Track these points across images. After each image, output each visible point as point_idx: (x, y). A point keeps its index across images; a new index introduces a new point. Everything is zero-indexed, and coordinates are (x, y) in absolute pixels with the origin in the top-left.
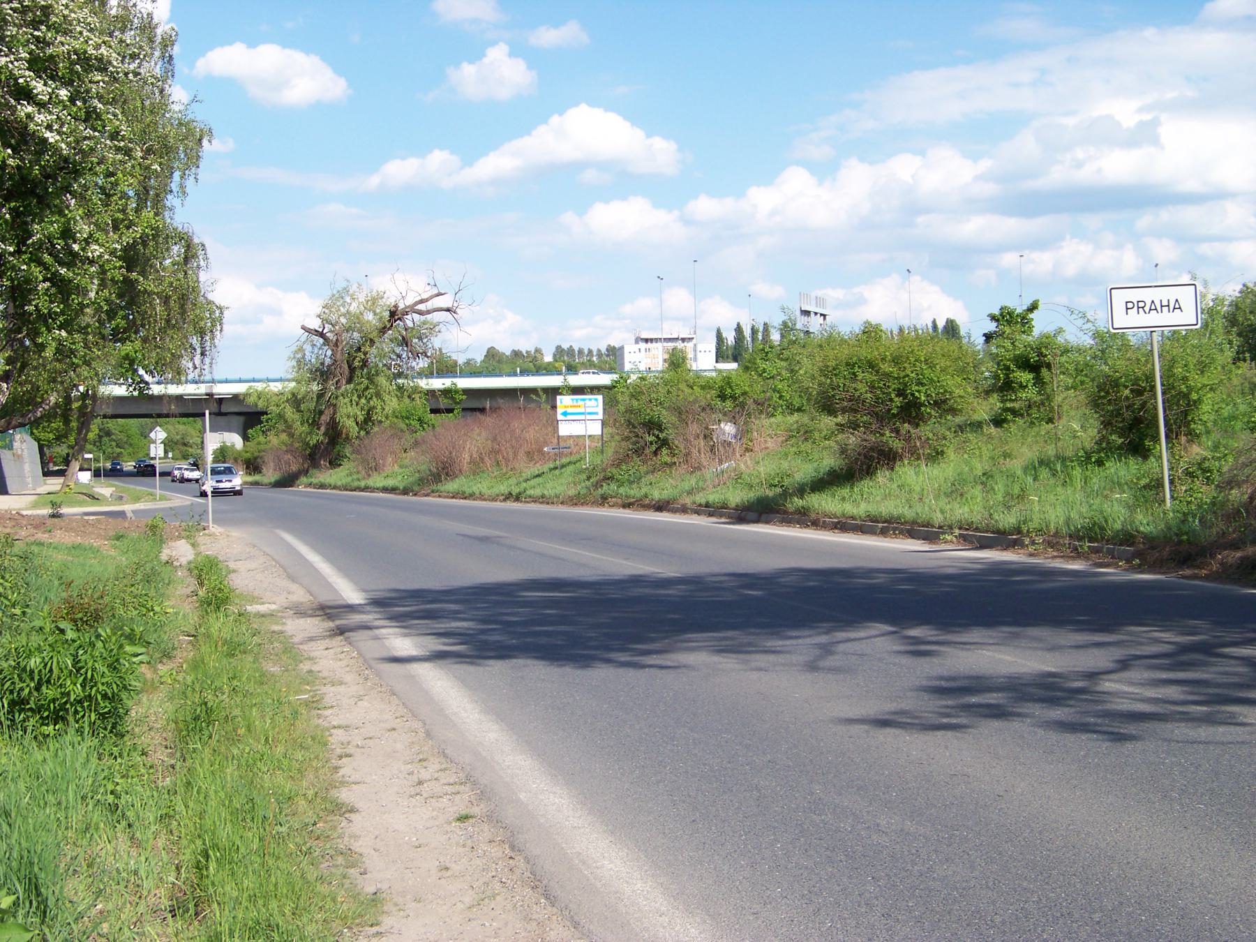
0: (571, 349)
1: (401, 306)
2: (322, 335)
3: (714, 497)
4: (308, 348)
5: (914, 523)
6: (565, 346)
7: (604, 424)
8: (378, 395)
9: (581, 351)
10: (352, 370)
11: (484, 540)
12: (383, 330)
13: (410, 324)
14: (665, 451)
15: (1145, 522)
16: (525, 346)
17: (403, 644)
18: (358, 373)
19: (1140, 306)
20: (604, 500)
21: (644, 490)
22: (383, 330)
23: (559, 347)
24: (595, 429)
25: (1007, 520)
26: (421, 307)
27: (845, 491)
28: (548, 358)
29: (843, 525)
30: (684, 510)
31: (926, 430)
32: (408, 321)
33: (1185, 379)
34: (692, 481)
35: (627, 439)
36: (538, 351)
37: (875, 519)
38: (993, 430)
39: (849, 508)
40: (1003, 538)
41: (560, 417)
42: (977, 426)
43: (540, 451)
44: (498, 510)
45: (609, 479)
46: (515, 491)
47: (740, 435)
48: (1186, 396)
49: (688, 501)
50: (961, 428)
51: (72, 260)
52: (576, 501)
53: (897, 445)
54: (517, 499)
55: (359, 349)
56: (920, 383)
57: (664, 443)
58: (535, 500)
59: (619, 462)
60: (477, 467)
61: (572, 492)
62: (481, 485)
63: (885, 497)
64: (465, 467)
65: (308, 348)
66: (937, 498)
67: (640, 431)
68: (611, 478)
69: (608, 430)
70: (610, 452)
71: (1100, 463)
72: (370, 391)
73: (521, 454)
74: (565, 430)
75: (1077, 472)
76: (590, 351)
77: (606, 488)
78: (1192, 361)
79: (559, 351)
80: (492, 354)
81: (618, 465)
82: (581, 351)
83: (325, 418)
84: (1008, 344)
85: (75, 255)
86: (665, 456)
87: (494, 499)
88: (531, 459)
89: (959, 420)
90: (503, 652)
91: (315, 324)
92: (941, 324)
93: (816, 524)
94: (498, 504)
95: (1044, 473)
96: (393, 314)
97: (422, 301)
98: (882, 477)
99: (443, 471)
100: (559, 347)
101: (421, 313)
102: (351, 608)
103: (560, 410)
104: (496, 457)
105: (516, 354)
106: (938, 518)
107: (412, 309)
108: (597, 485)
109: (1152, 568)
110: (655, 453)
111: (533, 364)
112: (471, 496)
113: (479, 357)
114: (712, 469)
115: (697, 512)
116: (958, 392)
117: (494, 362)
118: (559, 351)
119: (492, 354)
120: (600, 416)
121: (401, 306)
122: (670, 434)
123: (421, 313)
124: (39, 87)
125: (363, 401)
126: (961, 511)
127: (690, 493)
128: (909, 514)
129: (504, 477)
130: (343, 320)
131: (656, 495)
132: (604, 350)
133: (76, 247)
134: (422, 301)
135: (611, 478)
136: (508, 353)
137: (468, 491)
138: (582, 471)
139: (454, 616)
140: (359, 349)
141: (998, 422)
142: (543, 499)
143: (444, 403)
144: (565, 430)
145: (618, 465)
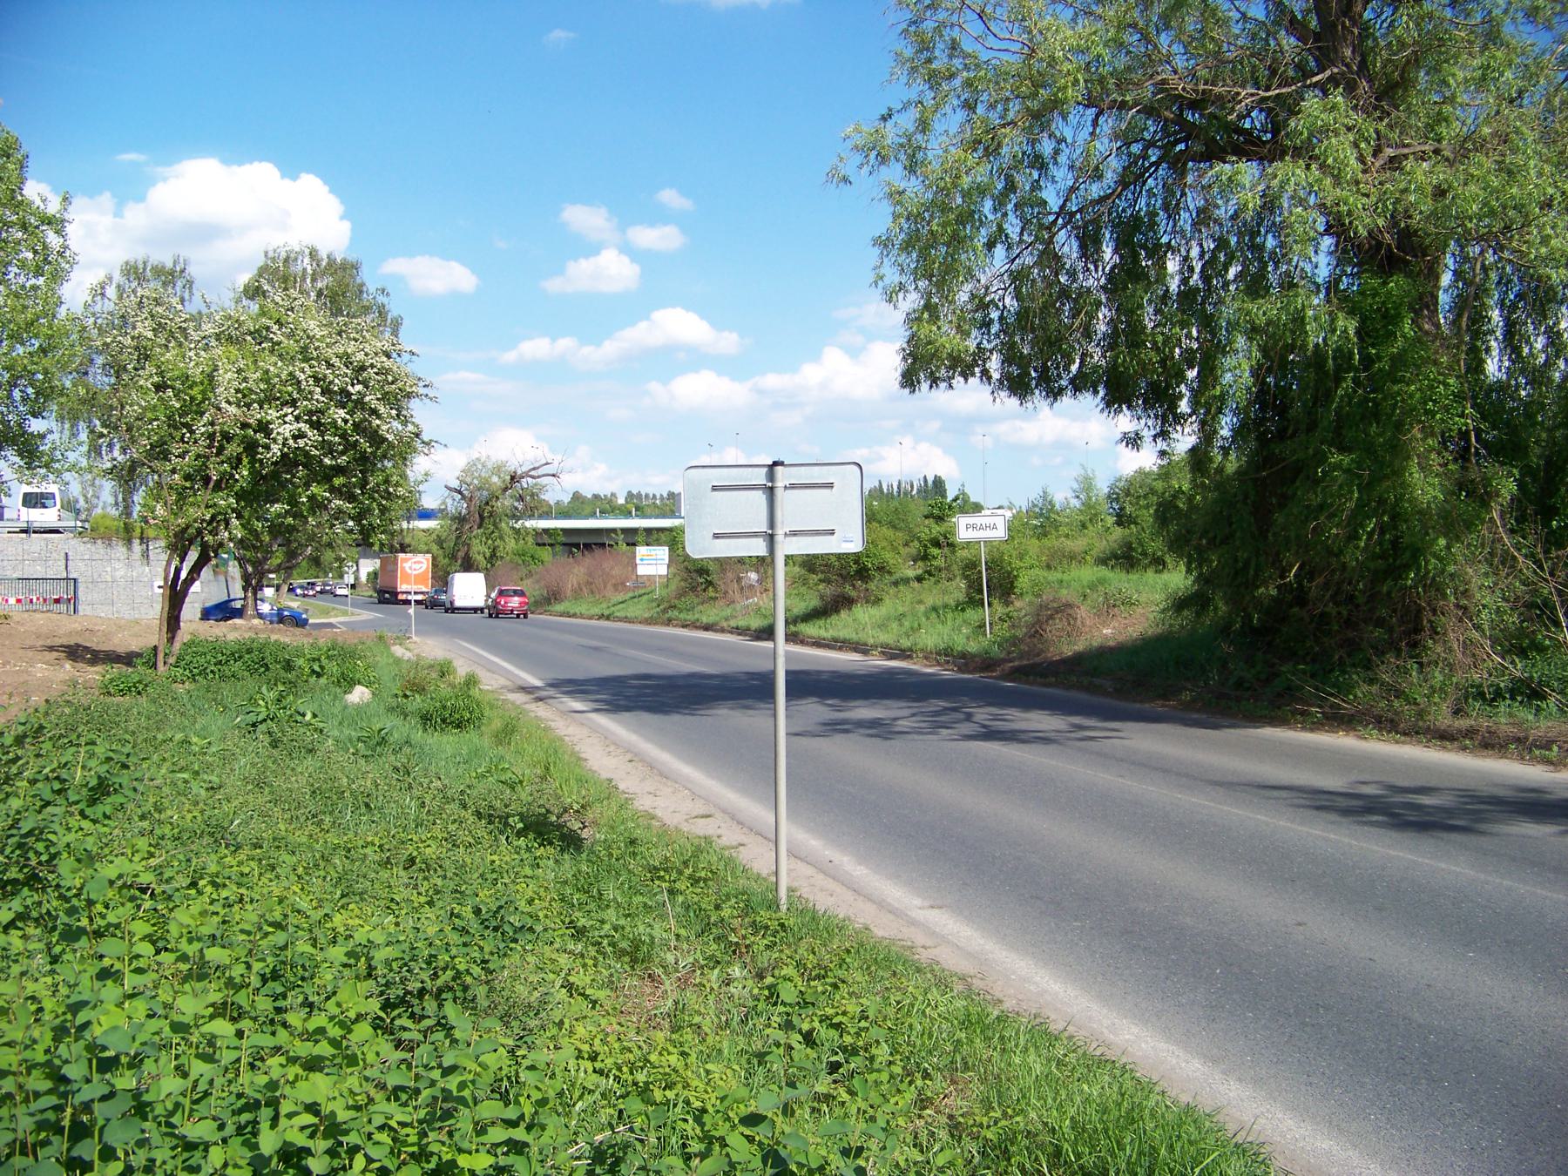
0: (639, 494)
1: (519, 472)
2: (460, 492)
3: (742, 623)
4: (449, 502)
5: (858, 643)
6: (635, 492)
7: (669, 566)
8: (501, 538)
9: (647, 496)
10: (482, 518)
11: (596, 649)
12: (506, 489)
13: (525, 486)
14: (711, 589)
15: (973, 647)
16: (604, 490)
17: (578, 706)
18: (487, 521)
19: (974, 527)
20: (669, 622)
21: (696, 616)
22: (506, 489)
23: (629, 492)
24: (663, 570)
25: (905, 643)
26: (533, 473)
27: (821, 622)
28: (621, 501)
29: (818, 643)
30: (723, 631)
31: (872, 586)
32: (524, 482)
33: (1010, 563)
34: (729, 611)
35: (686, 580)
36: (613, 495)
37: (836, 640)
38: (916, 585)
39: (823, 633)
40: (904, 654)
41: (638, 562)
42: (906, 581)
43: (623, 584)
44: (593, 627)
45: (673, 607)
46: (606, 613)
47: (760, 581)
48: (1010, 573)
49: (725, 624)
50: (896, 584)
51: (389, 496)
52: (649, 621)
53: (853, 594)
54: (608, 618)
55: (487, 503)
56: (868, 556)
57: (710, 583)
58: (620, 620)
59: (681, 594)
60: (577, 594)
61: (646, 615)
62: (582, 608)
63: (845, 627)
64: (569, 593)
65: (449, 502)
66: (873, 628)
67: (694, 575)
68: (675, 607)
69: (673, 570)
70: (673, 587)
71: (963, 610)
72: (494, 534)
73: (609, 586)
74: (642, 570)
75: (949, 616)
76: (654, 496)
77: (670, 614)
78: (1014, 553)
79: (630, 495)
80: (577, 497)
81: (679, 598)
82: (647, 496)
83: (461, 554)
84: (927, 531)
85: (389, 493)
86: (711, 592)
87: (591, 618)
88: (616, 590)
89: (894, 578)
90: (628, 709)
91: (455, 484)
92: (930, 480)
93: (802, 643)
94: (593, 622)
95: (934, 615)
96: (513, 478)
97: (534, 469)
98: (844, 614)
99: (551, 597)
100: (629, 492)
101: (533, 477)
102: (538, 688)
103: (638, 558)
104: (591, 587)
105: (596, 497)
106: (871, 641)
107: (527, 474)
108: (665, 611)
109: (970, 672)
110: (705, 590)
111: (606, 506)
112: (574, 616)
113: (566, 499)
114: (742, 603)
115: (731, 633)
116: (891, 562)
117: (579, 505)
118: (630, 495)
119: (577, 497)
120: (667, 561)
121: (519, 472)
122: (714, 577)
123: (533, 477)
124: (382, 410)
125: (490, 542)
126: (884, 638)
127: (726, 619)
128: (854, 637)
129: (598, 602)
130: (476, 482)
131: (705, 620)
132: (665, 495)
133: (391, 490)
134: (534, 469)
135: (675, 607)
136: (589, 496)
137: (572, 612)
138: (653, 600)
139: (597, 692)
140: (487, 503)
141: (919, 579)
142: (626, 620)
143: (546, 539)
144: (642, 570)
145: (679, 598)
